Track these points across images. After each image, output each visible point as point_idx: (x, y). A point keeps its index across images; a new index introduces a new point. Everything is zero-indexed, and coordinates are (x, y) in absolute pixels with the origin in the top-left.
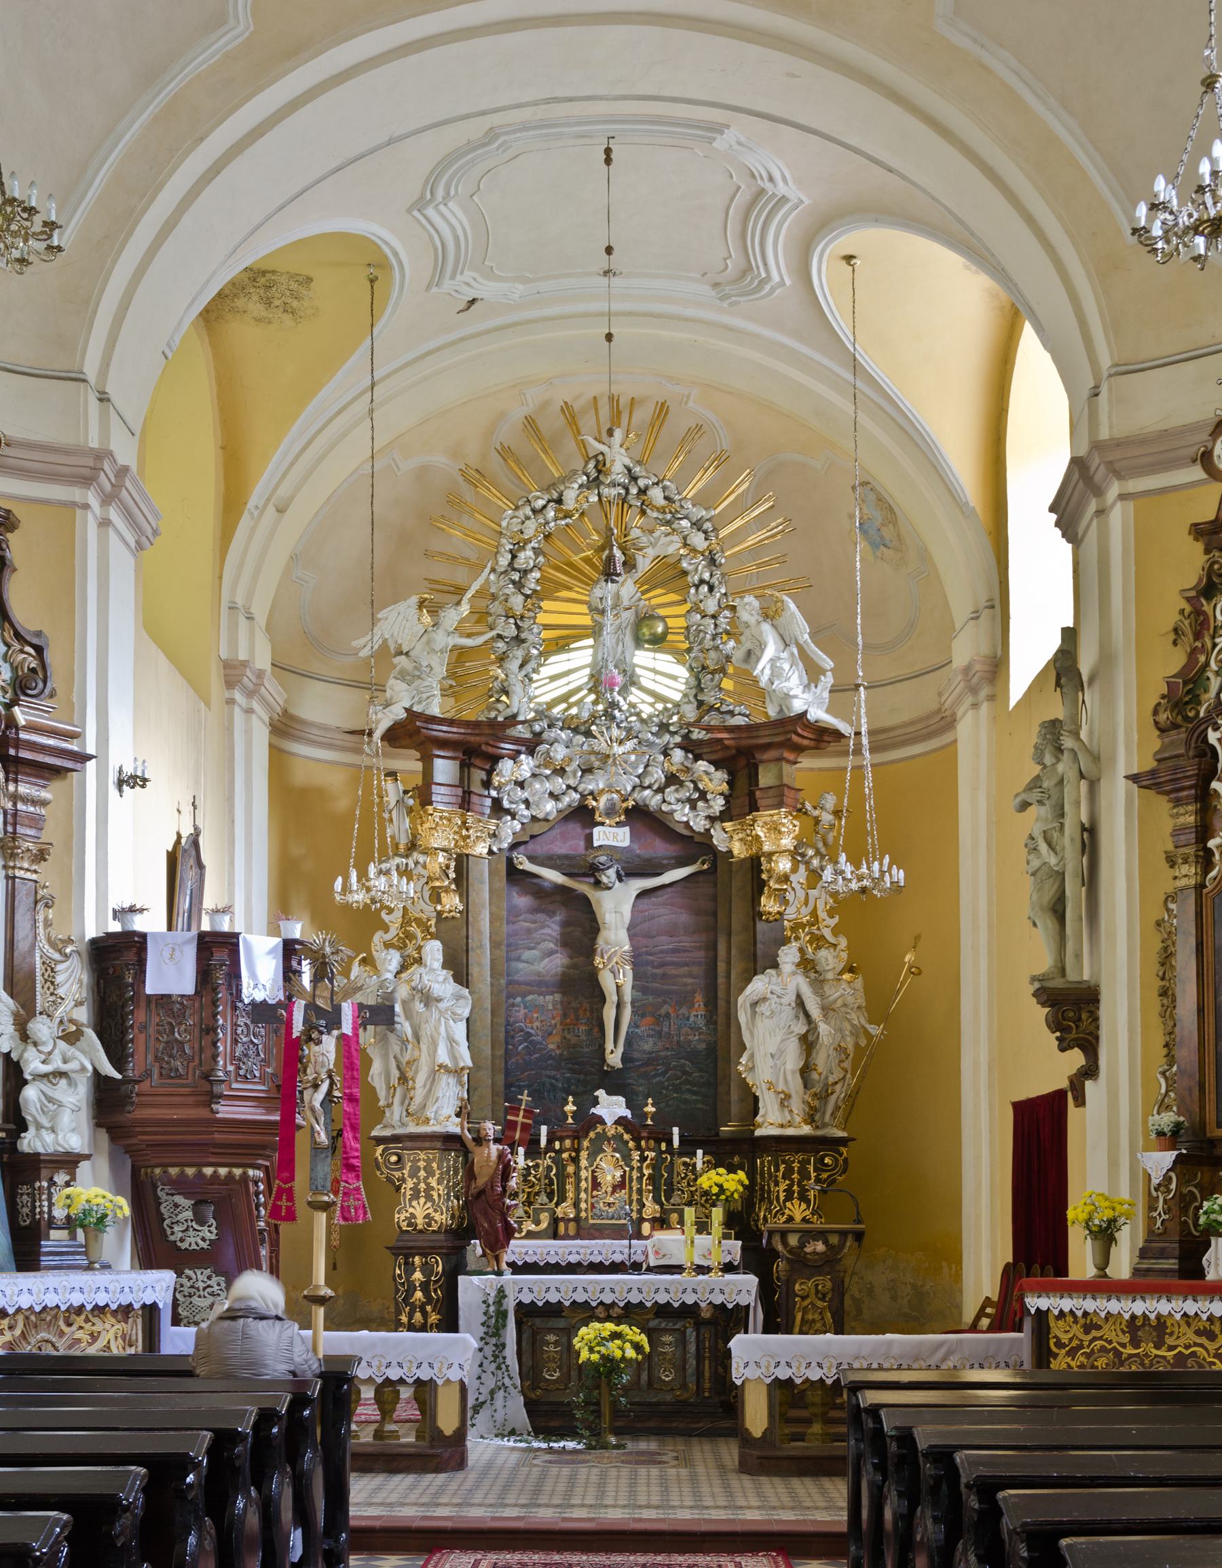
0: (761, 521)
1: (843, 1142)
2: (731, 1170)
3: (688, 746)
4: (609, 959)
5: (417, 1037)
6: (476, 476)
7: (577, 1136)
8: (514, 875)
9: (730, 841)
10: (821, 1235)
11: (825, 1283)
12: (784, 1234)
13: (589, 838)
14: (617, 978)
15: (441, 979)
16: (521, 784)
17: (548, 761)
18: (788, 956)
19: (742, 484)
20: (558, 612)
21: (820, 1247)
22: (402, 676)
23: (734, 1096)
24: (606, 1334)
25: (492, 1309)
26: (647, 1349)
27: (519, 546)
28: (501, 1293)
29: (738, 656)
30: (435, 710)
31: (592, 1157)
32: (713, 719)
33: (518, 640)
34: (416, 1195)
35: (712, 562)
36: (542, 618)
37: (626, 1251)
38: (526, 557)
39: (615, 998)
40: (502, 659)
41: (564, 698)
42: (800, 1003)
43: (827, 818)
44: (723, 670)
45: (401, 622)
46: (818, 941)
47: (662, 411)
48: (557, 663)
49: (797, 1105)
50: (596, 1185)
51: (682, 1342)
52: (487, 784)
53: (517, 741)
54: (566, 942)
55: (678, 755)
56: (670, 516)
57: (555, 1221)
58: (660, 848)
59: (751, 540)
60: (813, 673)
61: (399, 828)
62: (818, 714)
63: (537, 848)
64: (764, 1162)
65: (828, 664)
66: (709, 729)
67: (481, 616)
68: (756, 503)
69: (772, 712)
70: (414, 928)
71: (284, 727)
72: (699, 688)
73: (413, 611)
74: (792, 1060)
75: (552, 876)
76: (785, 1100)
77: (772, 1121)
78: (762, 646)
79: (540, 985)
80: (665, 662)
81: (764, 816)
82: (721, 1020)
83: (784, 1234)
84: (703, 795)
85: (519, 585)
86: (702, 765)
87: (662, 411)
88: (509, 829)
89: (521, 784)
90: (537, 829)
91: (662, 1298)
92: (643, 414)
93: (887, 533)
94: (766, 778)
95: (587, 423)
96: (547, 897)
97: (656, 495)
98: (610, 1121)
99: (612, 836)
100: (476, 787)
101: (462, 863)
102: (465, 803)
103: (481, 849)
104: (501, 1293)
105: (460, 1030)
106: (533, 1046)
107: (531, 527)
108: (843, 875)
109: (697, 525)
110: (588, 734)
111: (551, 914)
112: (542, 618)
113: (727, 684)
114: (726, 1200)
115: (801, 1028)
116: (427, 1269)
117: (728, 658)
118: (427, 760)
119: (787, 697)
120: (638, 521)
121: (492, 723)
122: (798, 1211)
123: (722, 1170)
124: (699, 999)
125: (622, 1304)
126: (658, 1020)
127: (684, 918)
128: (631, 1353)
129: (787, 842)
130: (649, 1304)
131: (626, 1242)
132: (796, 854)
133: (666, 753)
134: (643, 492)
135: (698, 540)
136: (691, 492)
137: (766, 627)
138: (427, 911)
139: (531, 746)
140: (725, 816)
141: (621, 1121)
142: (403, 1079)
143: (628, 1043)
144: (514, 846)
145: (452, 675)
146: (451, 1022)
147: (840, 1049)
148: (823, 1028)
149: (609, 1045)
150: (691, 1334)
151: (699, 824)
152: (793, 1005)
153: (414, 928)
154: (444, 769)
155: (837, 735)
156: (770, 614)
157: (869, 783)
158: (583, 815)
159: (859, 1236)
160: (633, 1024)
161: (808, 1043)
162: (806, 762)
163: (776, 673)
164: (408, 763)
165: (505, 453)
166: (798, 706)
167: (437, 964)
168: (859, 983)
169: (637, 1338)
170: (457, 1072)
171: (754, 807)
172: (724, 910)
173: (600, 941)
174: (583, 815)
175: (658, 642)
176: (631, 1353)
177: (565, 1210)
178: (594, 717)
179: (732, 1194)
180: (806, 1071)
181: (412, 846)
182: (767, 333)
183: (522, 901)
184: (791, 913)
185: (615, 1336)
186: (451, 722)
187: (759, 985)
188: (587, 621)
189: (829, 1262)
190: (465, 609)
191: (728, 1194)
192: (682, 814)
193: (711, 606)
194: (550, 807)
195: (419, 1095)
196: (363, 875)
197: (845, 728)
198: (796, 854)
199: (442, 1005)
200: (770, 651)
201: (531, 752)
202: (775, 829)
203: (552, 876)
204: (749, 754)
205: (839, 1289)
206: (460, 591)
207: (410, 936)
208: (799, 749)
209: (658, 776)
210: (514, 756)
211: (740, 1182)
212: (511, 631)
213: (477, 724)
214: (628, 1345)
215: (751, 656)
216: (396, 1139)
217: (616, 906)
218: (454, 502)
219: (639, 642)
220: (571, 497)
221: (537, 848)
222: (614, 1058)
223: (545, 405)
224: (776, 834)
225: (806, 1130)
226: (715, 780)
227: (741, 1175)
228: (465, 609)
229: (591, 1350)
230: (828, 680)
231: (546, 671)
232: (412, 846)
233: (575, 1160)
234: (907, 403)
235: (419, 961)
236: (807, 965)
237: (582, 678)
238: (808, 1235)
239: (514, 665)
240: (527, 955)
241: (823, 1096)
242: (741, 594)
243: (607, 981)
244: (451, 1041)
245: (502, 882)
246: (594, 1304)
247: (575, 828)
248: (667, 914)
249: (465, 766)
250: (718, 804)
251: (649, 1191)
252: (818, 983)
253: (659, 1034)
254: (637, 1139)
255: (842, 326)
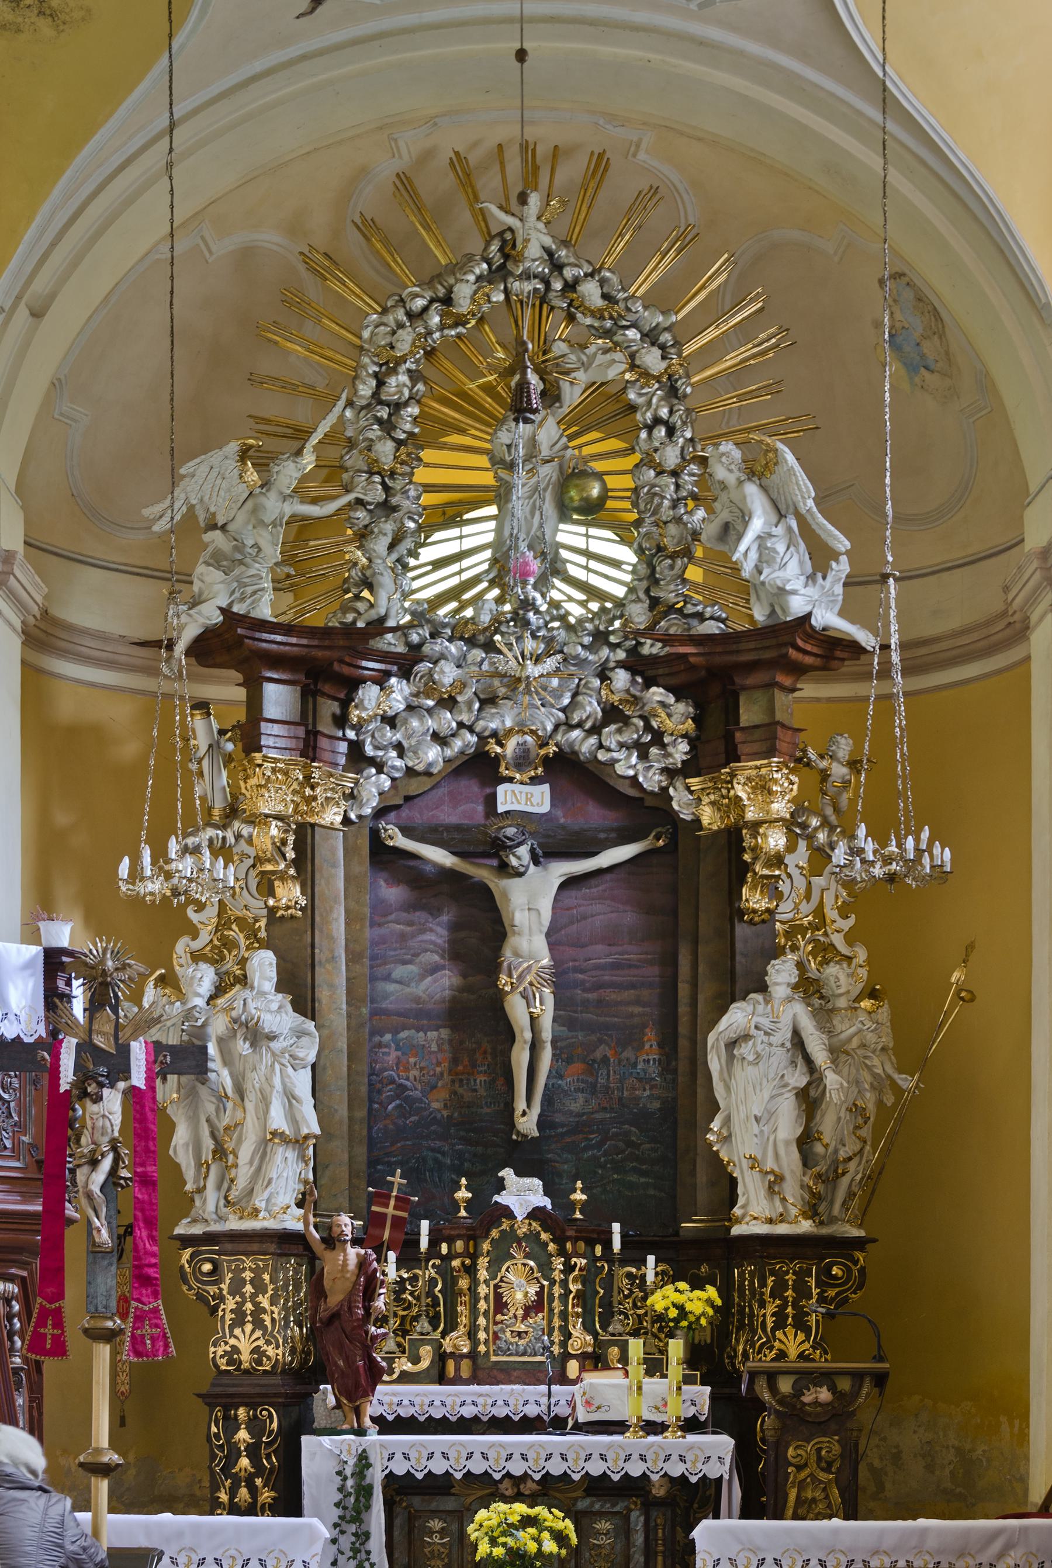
0: (744, 332)
1: (859, 1244)
2: (697, 1284)
3: (635, 664)
4: (521, 978)
5: (240, 1092)
6: (324, 263)
7: (474, 1235)
8: (381, 855)
9: (695, 805)
10: (826, 1378)
11: (831, 1446)
12: (772, 1377)
13: (491, 801)
14: (532, 1008)
15: (274, 1006)
16: (391, 721)
17: (430, 687)
18: (782, 974)
19: (717, 276)
20: (442, 467)
21: (824, 1395)
22: (217, 560)
23: (702, 1177)
24: (514, 1519)
25: (350, 1483)
26: (574, 1540)
27: (389, 367)
28: (363, 1461)
29: (709, 532)
30: (265, 611)
31: (494, 1267)
32: (671, 625)
33: (387, 508)
34: (239, 1320)
35: (672, 392)
36: (422, 475)
37: (544, 1400)
38: (398, 383)
39: (528, 1035)
40: (363, 536)
41: (453, 594)
42: (798, 1041)
43: (839, 771)
44: (687, 553)
45: (215, 480)
46: (825, 952)
47: (600, 165)
48: (444, 543)
49: (791, 1190)
50: (501, 1306)
51: (625, 1531)
52: (341, 721)
53: (385, 657)
54: (456, 953)
55: (621, 678)
56: (611, 323)
57: (441, 1357)
58: (594, 816)
59: (730, 360)
60: (820, 558)
61: (214, 784)
62: (827, 617)
63: (413, 814)
64: (744, 1273)
65: (842, 543)
66: (667, 640)
67: (332, 472)
68: (737, 304)
69: (760, 614)
70: (235, 933)
71: (43, 636)
72: (653, 580)
73: (232, 465)
74: (787, 1125)
75: (438, 856)
76: (774, 1184)
77: (755, 1214)
78: (745, 517)
79: (418, 1016)
80: (604, 542)
81: (748, 768)
82: (683, 1066)
83: (772, 1377)
84: (658, 738)
85: (388, 426)
86: (657, 693)
87: (600, 165)
88: (374, 787)
89: (391, 721)
90: (415, 787)
91: (596, 1468)
92: (571, 172)
93: (930, 348)
94: (749, 714)
95: (489, 183)
96: (427, 887)
97: (591, 291)
98: (520, 1214)
99: (524, 797)
100: (326, 727)
101: (305, 836)
102: (309, 748)
103: (333, 816)
104: (363, 1461)
105: (302, 1082)
106: (409, 1106)
107: (405, 340)
108: (860, 854)
109: (651, 337)
110: (490, 647)
111: (435, 912)
112: (422, 475)
113: (694, 573)
114: (689, 1327)
115: (799, 1079)
116: (255, 1426)
117: (696, 535)
118: (254, 687)
119: (782, 592)
120: (563, 330)
121: (349, 630)
122: (792, 1343)
123: (682, 1285)
124: (651, 1038)
125: (537, 1477)
126: (592, 1067)
127: (629, 918)
128: (550, 1546)
129: (780, 807)
130: (576, 1477)
131: (544, 1388)
132: (794, 826)
133: (603, 675)
134: (571, 286)
135: (652, 360)
136: (641, 287)
137: (751, 489)
138: (255, 906)
139: (406, 664)
140: (688, 769)
141: (536, 1214)
142: (220, 1152)
143: (548, 1100)
144: (380, 813)
145: (288, 558)
146: (290, 1069)
147: (855, 1109)
148: (831, 1079)
149: (521, 1104)
150: (637, 1520)
151: (651, 781)
152: (788, 1045)
153: (235, 933)
154: (278, 698)
155: (855, 649)
156: (758, 468)
157: (900, 720)
158: (481, 767)
159: (880, 1380)
160: (555, 1073)
161: (809, 1100)
162: (809, 689)
163: (766, 555)
164: (226, 690)
165: (367, 227)
166: (797, 606)
167: (269, 986)
168: (884, 1014)
169: (560, 1525)
170: (299, 1142)
171: (732, 756)
172: (690, 913)
173: (507, 953)
174: (481, 767)
175: (592, 512)
176: (550, 1546)
177: (457, 1341)
178: (497, 623)
179: (698, 1319)
180: (805, 1141)
181: (232, 812)
182: (753, 48)
183: (393, 893)
184: (785, 910)
185: (528, 1521)
186: (287, 629)
187: (737, 1016)
188: (487, 479)
189: (836, 1417)
190: (308, 460)
191: (692, 1318)
192: (627, 765)
193: (671, 457)
194: (433, 754)
195: (243, 1175)
196: (160, 855)
197: (865, 638)
198: (794, 826)
199: (275, 1045)
200: (757, 525)
201: (406, 674)
202: (763, 788)
203: (438, 856)
204: (728, 677)
205: (852, 1455)
206: (301, 434)
207: (229, 944)
208: (799, 670)
209: (591, 708)
210: (381, 680)
211: (710, 1302)
212: (377, 494)
213: (325, 632)
214: (546, 1535)
215: (730, 532)
216: (210, 1238)
217: (531, 900)
218: (293, 302)
219: (564, 513)
220: (464, 293)
221: (413, 814)
222: (528, 1123)
223: (427, 156)
224: (766, 797)
225: (806, 1226)
226: (675, 715)
227: (712, 1292)
228: (308, 460)
229: (493, 1542)
230: (842, 568)
231: (427, 554)
232: (232, 812)
233: (471, 1270)
234: (961, 153)
235: (243, 980)
236: (808, 987)
237: (479, 563)
238: (807, 1378)
239: (380, 545)
240: (400, 971)
241: (831, 1177)
242: (715, 439)
243: (518, 1010)
244: (290, 1097)
245: (363, 865)
246: (497, 1476)
247: (470, 787)
248: (601, 912)
249: (309, 695)
250: (680, 751)
251: (578, 1315)
252: (824, 1014)
253: (593, 1089)
254: (559, 1240)
255: (866, 37)
